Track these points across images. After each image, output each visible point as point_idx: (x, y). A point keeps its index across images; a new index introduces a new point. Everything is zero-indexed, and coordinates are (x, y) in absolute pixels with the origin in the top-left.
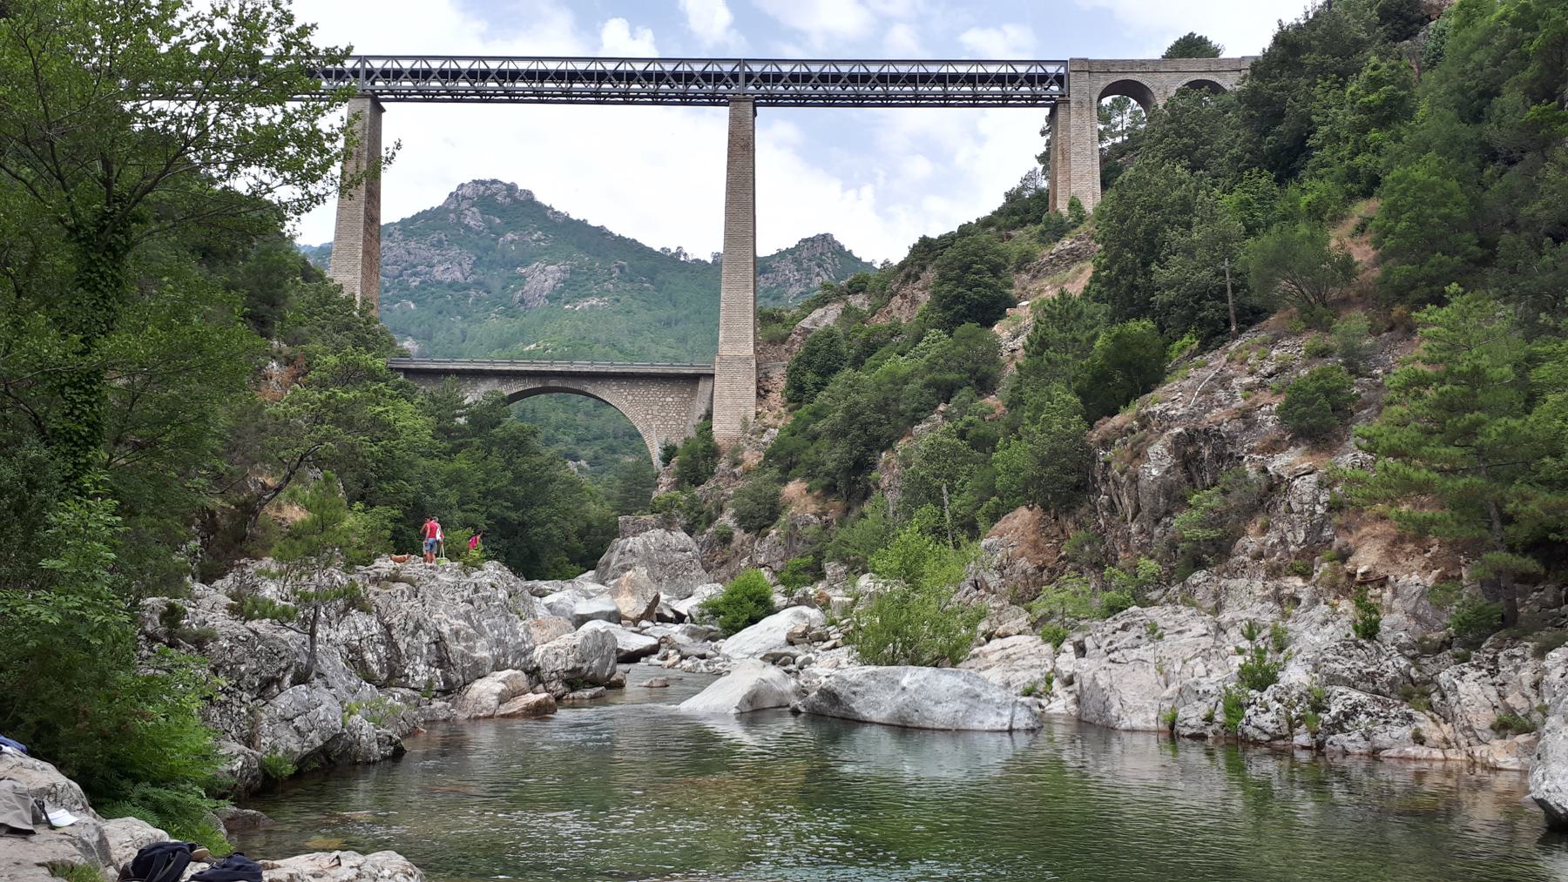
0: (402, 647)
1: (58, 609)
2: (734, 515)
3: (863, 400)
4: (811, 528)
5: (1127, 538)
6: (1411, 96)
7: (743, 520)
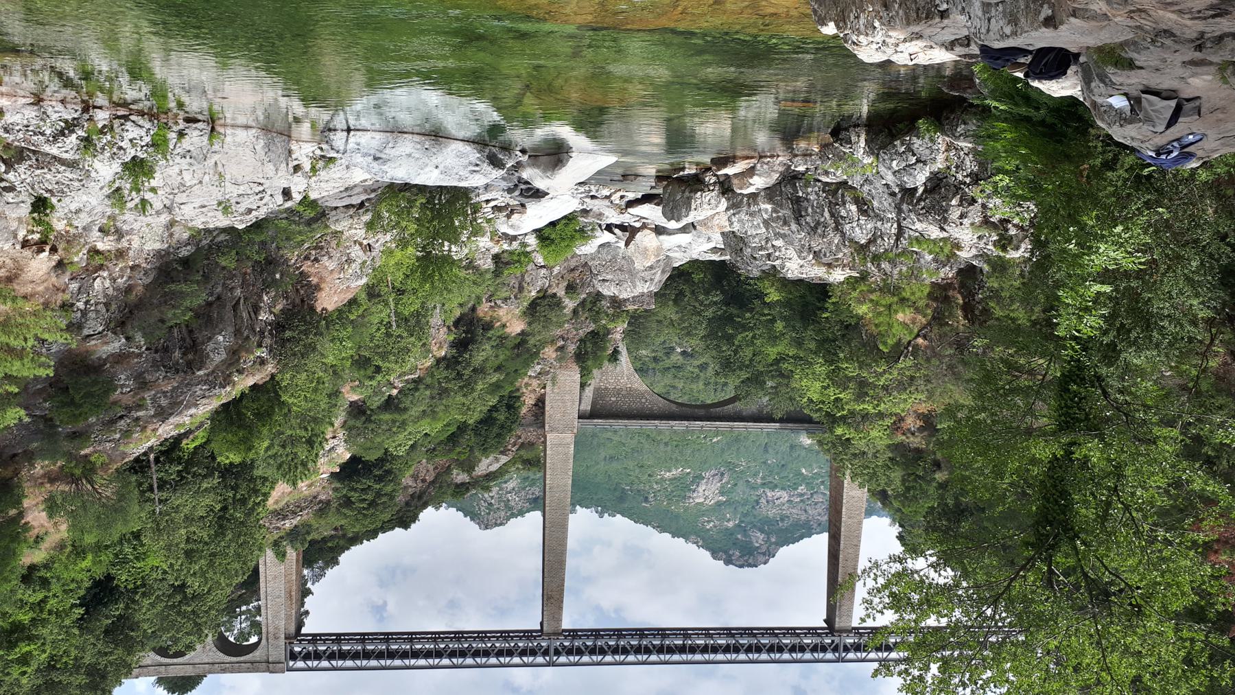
0: (827, 214)
3: (459, 398)
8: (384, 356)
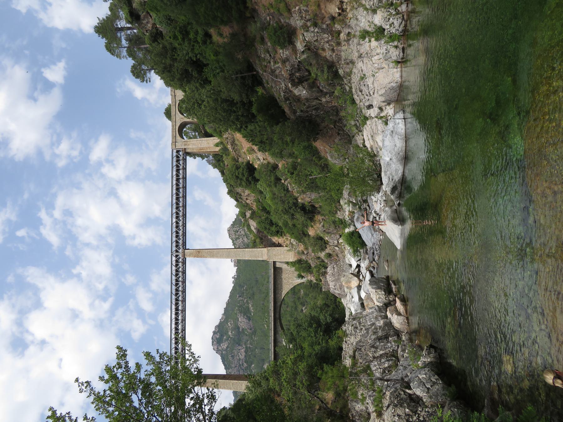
0: (382, 352)
3: (281, 208)
5: (327, 102)
7: (322, 249)
8: (298, 175)
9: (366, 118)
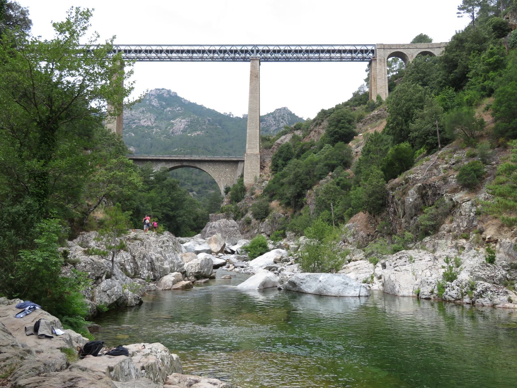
0: (139, 264)
1: (41, 256)
2: (252, 214)
3: (301, 171)
4: (281, 219)
6: (505, 59)
9: (375, 263)
